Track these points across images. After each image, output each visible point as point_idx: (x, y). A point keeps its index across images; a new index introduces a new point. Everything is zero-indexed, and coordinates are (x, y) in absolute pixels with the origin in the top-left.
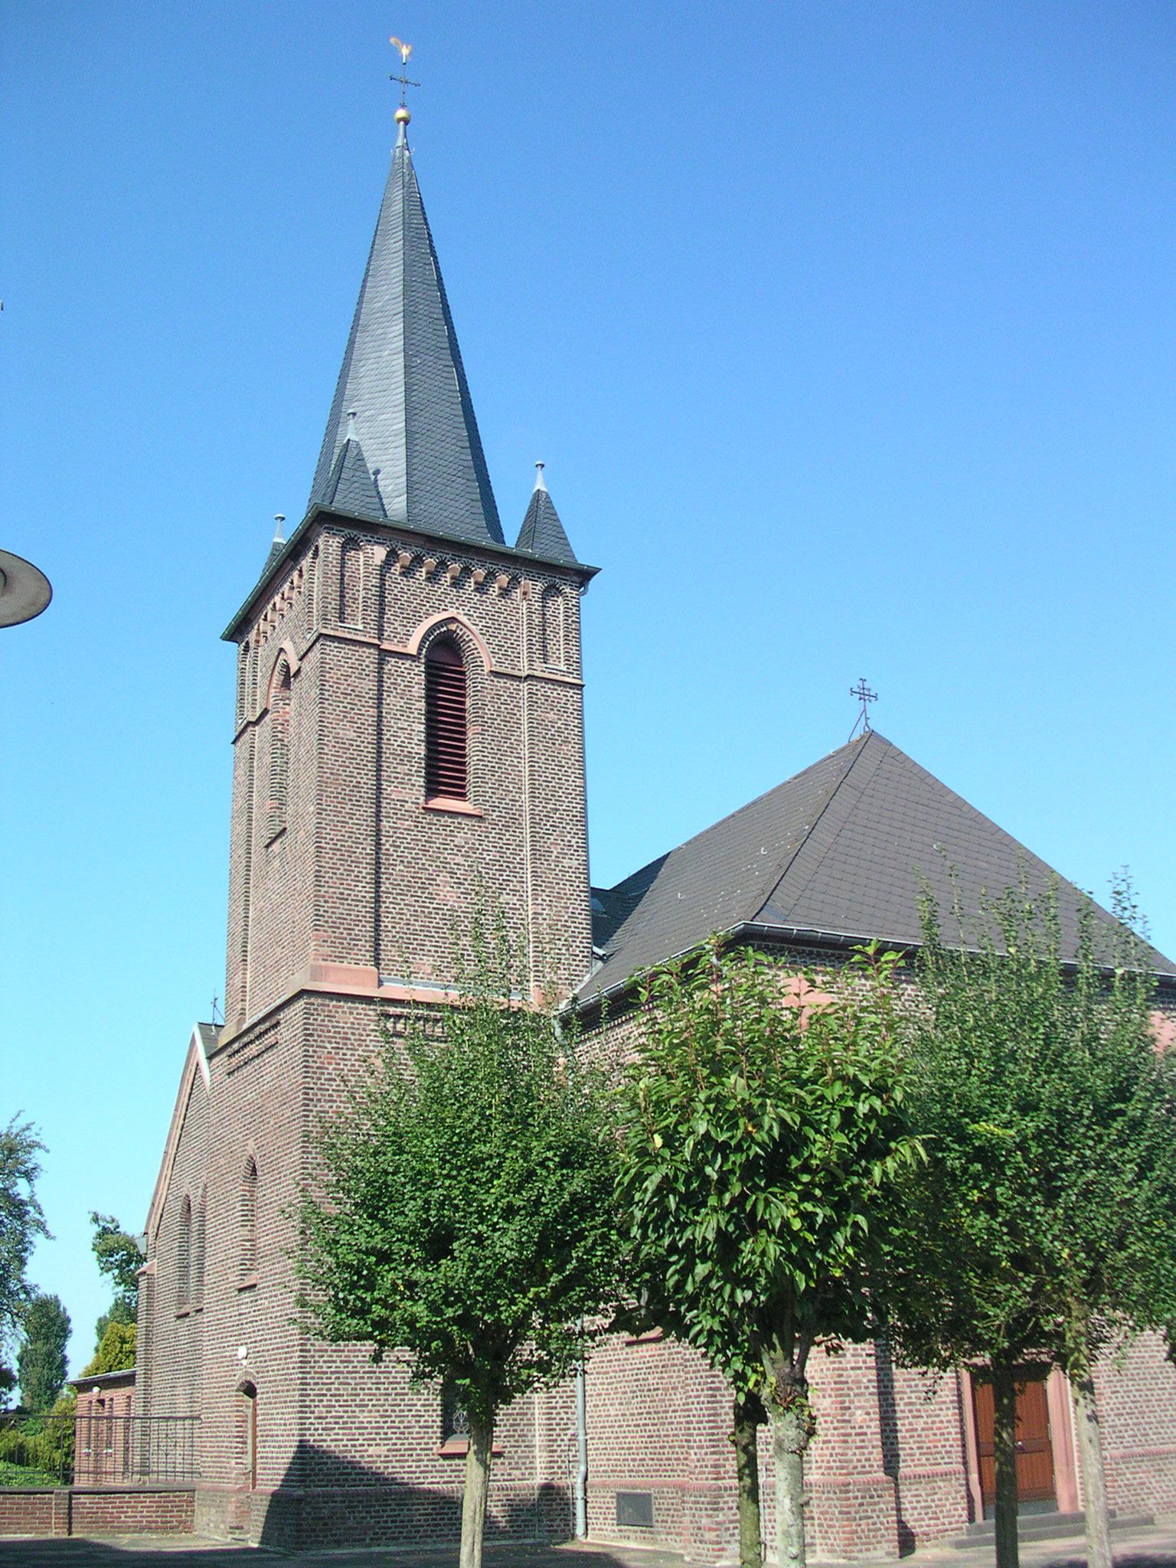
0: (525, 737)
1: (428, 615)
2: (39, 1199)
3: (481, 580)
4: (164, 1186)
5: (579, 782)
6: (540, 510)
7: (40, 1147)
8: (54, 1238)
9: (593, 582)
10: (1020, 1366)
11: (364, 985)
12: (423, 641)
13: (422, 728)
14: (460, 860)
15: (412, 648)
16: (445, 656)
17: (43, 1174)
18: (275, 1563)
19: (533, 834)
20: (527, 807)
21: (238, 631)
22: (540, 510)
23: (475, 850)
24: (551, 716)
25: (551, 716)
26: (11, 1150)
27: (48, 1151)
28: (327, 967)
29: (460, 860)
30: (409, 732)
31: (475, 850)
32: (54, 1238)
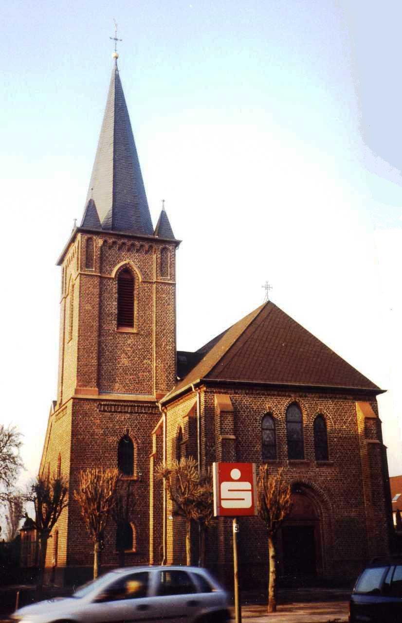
0: (154, 304)
1: (119, 263)
2: (21, 455)
3: (138, 248)
4: (44, 458)
5: (173, 319)
6: (163, 218)
7: (22, 434)
8: (27, 470)
9: (181, 246)
10: (52, 512)
11: (93, 395)
12: (117, 272)
13: (116, 303)
14: (129, 349)
15: (113, 275)
16: (126, 279)
17: (23, 446)
18: (253, 620)
19: (156, 338)
20: (154, 329)
21: (61, 262)
22: (163, 218)
23: (134, 345)
24: (164, 296)
25: (164, 296)
26: (10, 436)
27: (24, 436)
28: (80, 390)
29: (129, 349)
30: (113, 306)
31: (134, 345)
32: (27, 470)
